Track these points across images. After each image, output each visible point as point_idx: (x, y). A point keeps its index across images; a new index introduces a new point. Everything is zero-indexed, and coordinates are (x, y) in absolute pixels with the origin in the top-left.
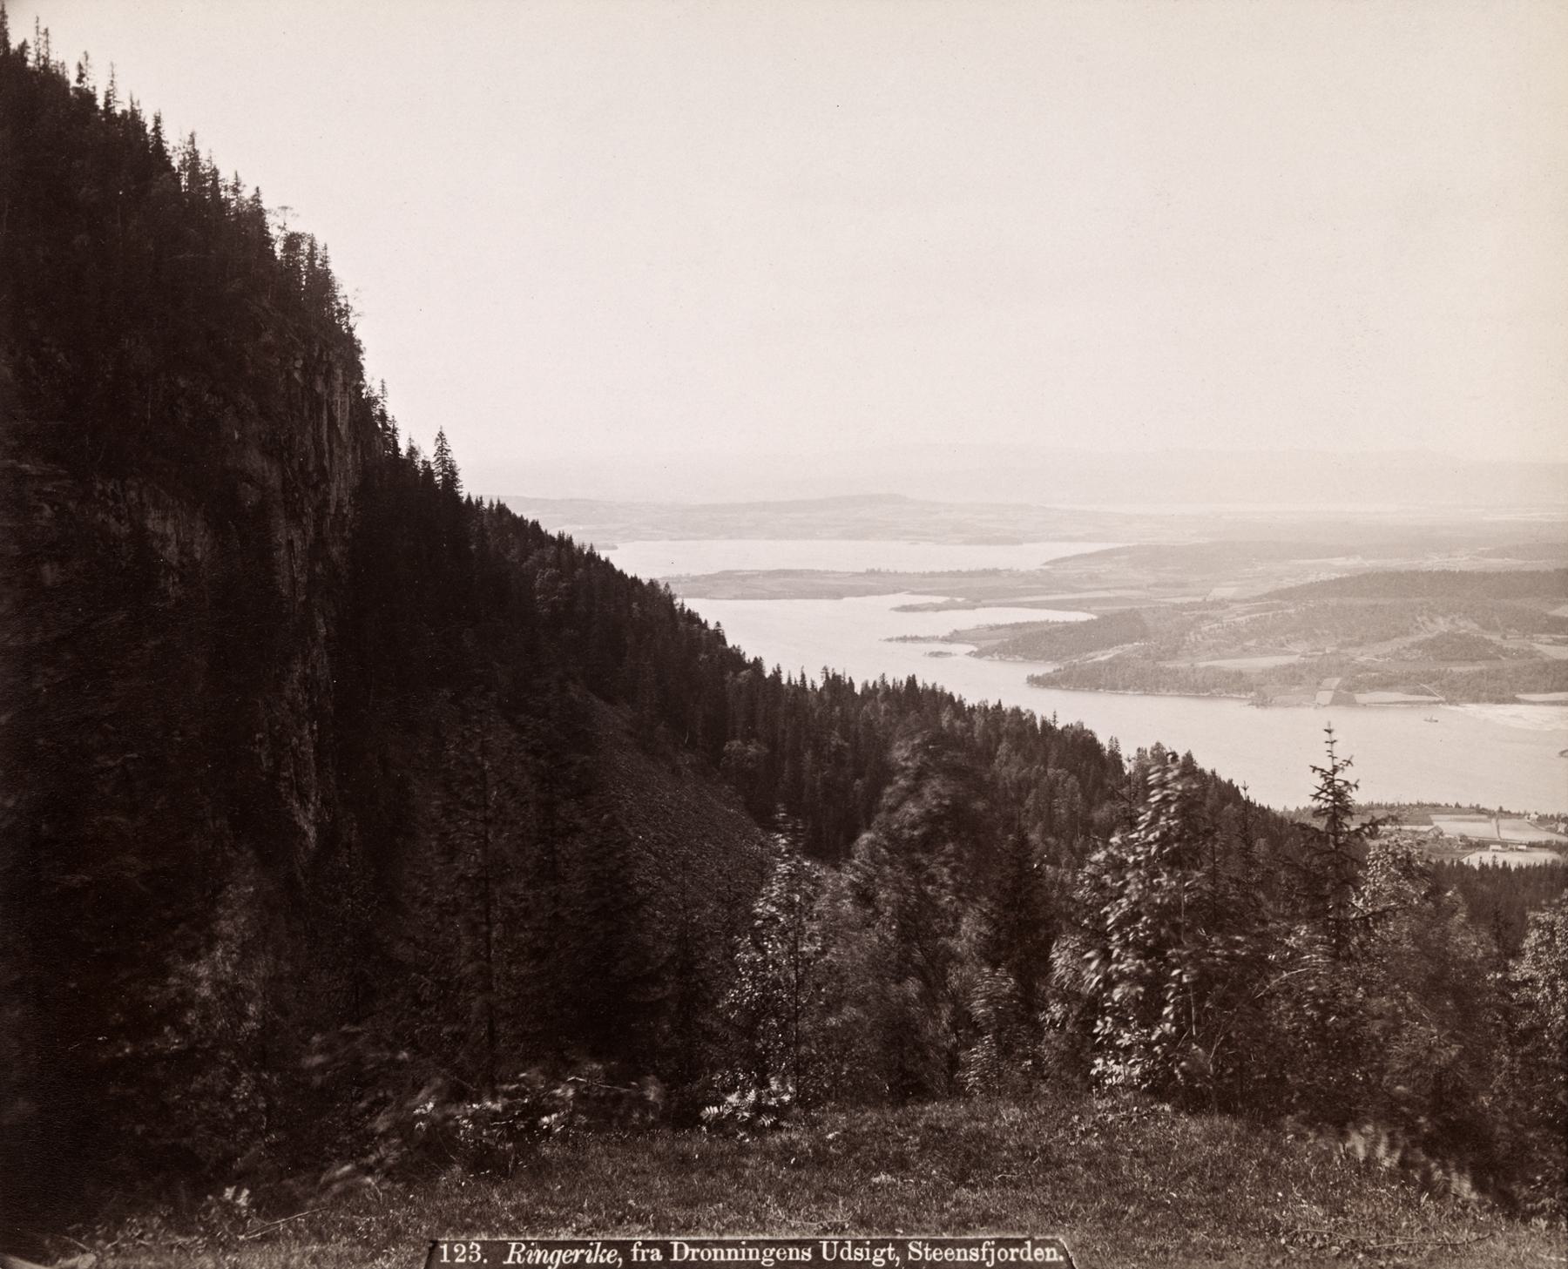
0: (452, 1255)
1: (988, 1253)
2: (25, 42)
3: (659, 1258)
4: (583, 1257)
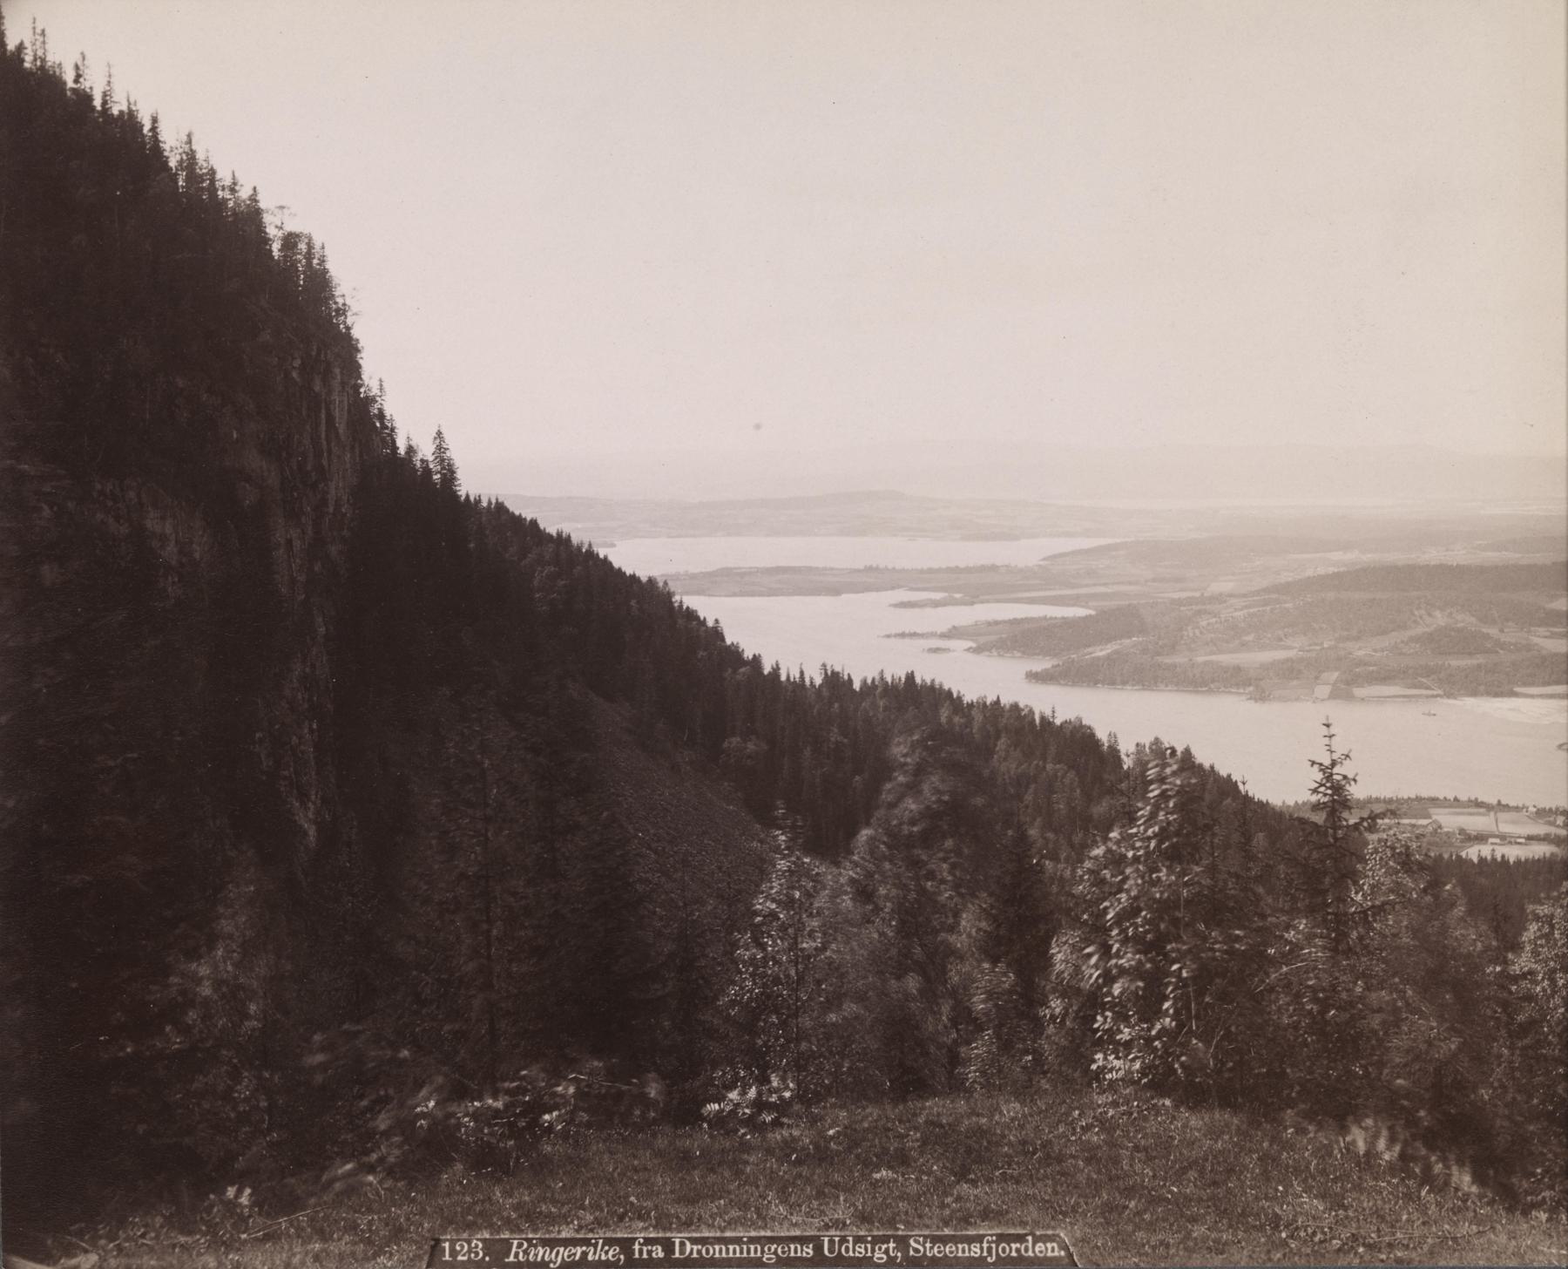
0: (454, 1253)
1: (990, 1249)
3: (661, 1255)
4: (585, 1254)
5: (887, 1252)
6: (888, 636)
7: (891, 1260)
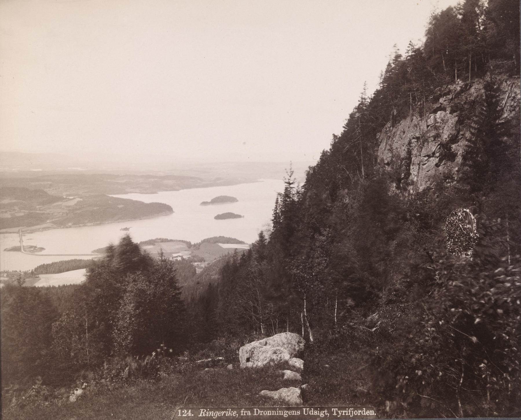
0: (182, 414)
1: (351, 412)
2: (237, 201)
3: (250, 414)
4: (225, 414)
5: (324, 413)
6: (204, 203)
7: (326, 416)
